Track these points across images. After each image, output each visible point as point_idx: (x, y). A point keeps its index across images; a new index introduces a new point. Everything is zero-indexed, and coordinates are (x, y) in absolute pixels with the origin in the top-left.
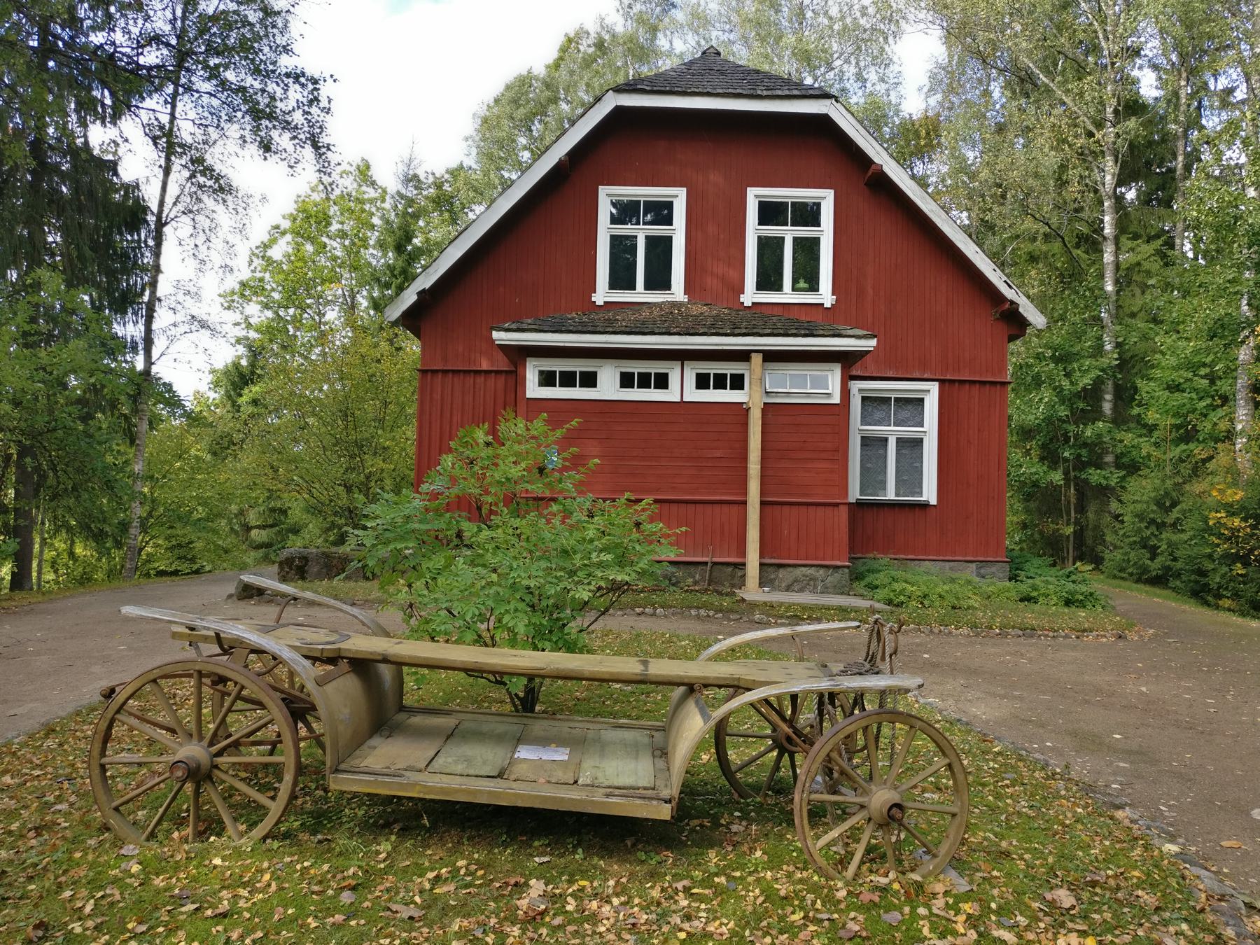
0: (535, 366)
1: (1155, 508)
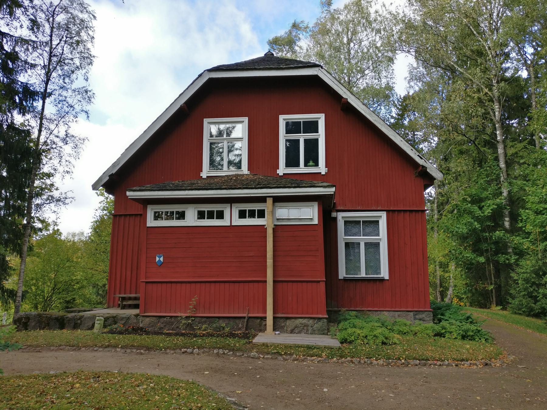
0: (152, 209)
1: (534, 276)
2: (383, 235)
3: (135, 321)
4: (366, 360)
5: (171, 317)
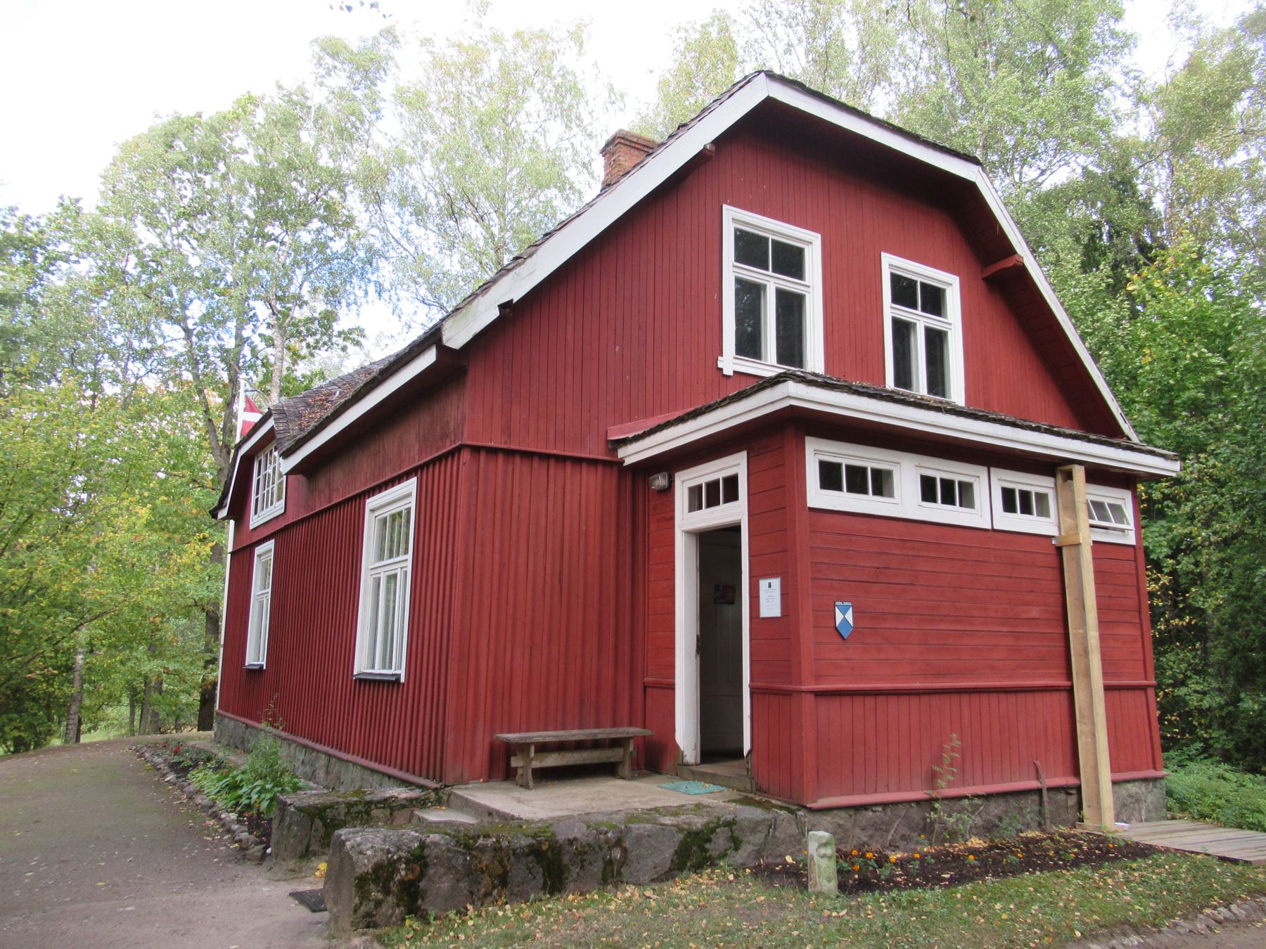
5: (885, 805)
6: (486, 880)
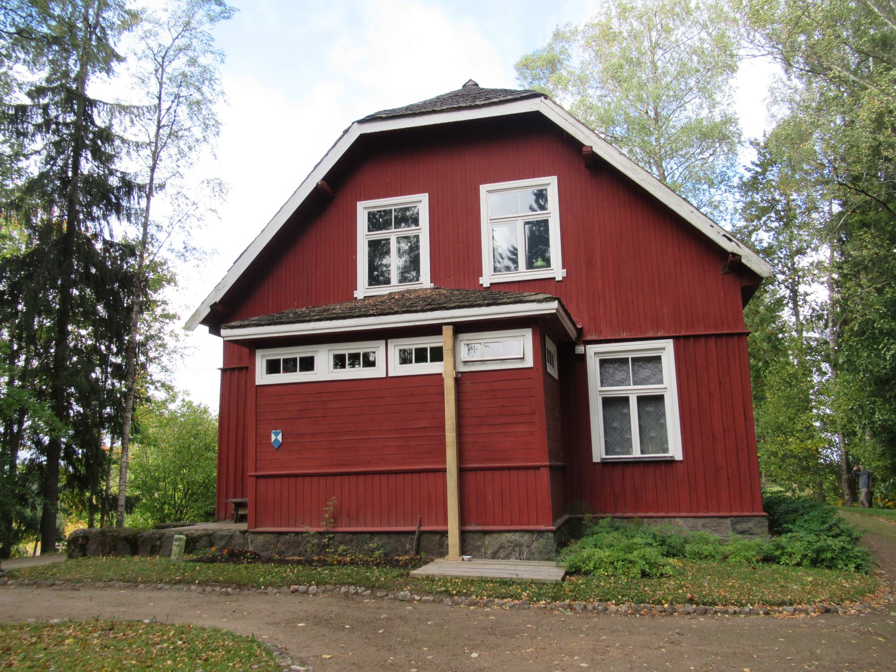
0: (263, 356)
2: (668, 384)
3: (242, 541)
4: (596, 604)
5: (297, 533)
6: (108, 547)
